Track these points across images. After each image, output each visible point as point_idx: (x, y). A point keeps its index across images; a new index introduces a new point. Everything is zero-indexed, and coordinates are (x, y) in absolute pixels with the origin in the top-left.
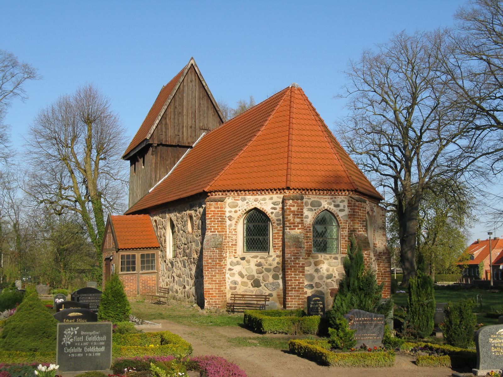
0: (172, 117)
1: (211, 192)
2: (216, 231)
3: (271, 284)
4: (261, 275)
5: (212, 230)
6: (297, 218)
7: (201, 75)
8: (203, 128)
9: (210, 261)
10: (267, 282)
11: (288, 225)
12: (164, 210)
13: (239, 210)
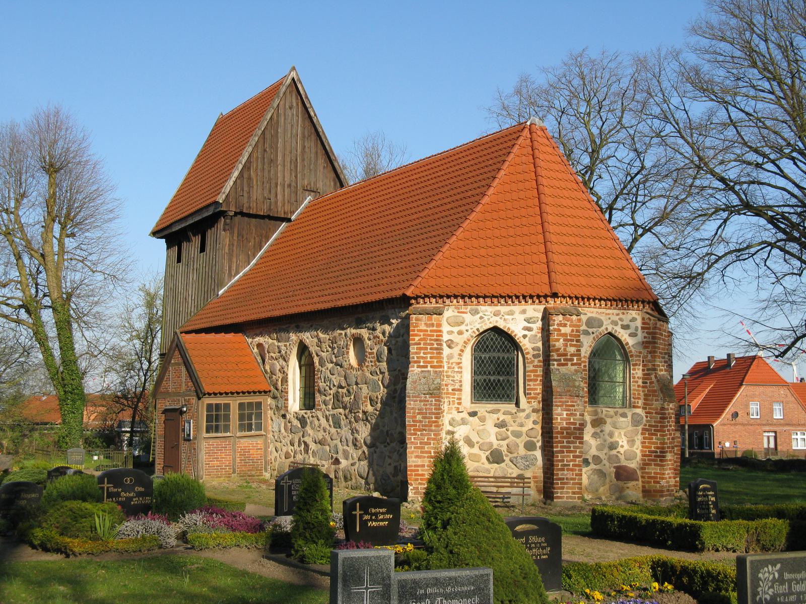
0: (260, 167)
1: (416, 298)
2: (429, 365)
3: (522, 458)
4: (504, 443)
5: (422, 364)
6: (571, 345)
7: (307, 97)
8: (309, 188)
9: (419, 417)
10: (515, 455)
11: (556, 357)
12: (284, 327)
13: (467, 331)
